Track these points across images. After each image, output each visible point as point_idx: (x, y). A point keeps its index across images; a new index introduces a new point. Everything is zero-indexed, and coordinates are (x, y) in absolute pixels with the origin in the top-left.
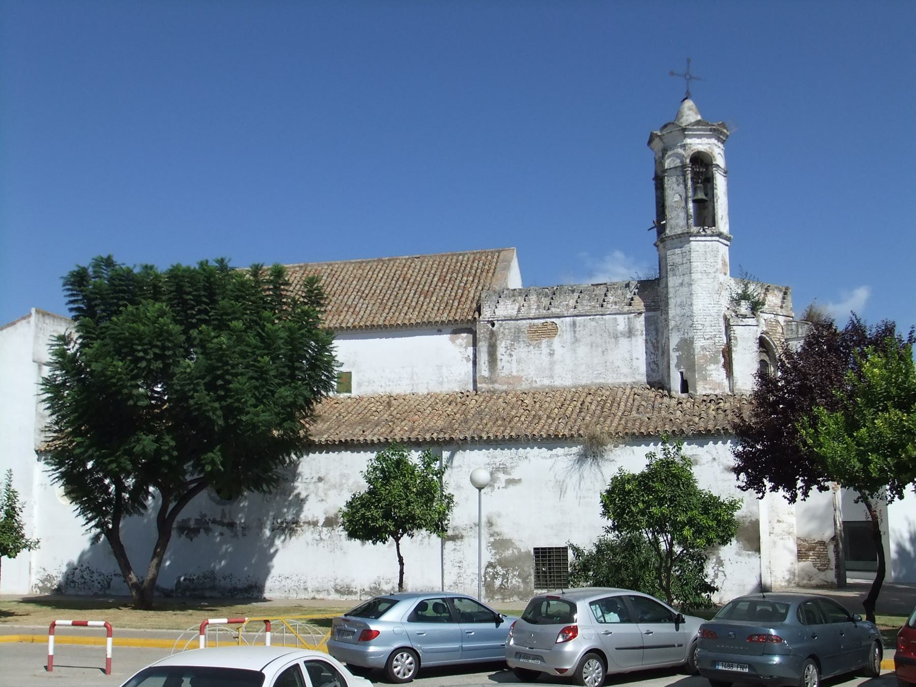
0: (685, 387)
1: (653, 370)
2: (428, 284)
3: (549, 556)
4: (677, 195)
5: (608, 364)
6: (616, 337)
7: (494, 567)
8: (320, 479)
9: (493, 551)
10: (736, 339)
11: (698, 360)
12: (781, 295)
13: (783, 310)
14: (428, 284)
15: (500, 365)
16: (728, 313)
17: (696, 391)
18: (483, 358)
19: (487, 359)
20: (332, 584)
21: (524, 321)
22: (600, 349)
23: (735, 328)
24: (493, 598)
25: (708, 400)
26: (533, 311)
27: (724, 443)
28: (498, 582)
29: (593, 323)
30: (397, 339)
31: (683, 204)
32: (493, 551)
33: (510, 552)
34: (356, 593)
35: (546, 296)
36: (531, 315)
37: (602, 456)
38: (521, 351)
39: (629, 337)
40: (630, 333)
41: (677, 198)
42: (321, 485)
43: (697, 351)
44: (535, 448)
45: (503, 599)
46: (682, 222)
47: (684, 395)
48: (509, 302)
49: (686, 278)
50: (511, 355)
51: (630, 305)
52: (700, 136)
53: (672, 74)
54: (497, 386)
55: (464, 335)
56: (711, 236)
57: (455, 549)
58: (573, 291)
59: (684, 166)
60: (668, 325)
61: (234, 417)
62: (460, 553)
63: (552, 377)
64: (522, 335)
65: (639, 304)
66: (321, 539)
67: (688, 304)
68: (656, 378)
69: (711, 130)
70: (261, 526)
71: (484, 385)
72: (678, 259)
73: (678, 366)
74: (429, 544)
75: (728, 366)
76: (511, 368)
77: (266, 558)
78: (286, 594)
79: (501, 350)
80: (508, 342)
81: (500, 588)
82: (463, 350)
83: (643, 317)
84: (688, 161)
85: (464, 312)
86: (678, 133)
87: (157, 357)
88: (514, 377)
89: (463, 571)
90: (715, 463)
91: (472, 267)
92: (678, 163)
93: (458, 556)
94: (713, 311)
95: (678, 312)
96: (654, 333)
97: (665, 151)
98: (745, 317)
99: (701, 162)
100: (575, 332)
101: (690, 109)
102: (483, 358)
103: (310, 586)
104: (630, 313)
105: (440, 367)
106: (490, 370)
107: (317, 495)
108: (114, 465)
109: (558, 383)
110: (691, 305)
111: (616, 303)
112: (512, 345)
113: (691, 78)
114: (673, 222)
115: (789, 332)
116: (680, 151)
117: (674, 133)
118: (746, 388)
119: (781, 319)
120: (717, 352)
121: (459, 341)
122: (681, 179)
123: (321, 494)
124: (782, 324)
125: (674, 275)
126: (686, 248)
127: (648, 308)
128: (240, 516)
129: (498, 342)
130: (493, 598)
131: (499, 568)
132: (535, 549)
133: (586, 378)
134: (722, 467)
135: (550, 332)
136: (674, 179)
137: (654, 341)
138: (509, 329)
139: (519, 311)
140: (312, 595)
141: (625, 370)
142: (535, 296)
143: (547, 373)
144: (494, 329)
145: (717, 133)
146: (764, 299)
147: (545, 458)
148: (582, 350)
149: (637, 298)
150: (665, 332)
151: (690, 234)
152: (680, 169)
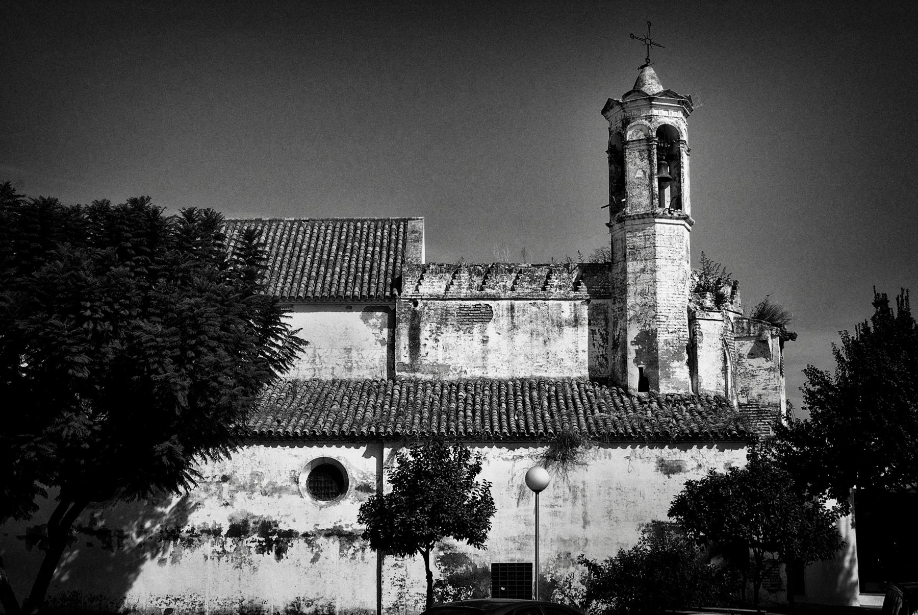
0: (644, 384)
2: (325, 253)
5: (550, 355)
6: (560, 326)
8: (225, 479)
9: (443, 568)
13: (733, 306)
14: (325, 253)
15: (423, 351)
17: (658, 390)
18: (403, 341)
19: (407, 343)
20: (237, 606)
21: (454, 302)
22: (541, 339)
25: (673, 400)
26: (464, 291)
29: (534, 309)
30: (303, 314)
31: (647, 182)
32: (443, 568)
35: (479, 274)
36: (462, 296)
38: (449, 335)
39: (575, 326)
41: (640, 174)
42: (225, 485)
43: (660, 345)
46: (645, 201)
47: (643, 394)
48: (436, 279)
50: (436, 340)
51: (576, 289)
52: (666, 108)
54: (419, 375)
55: (379, 314)
56: (677, 219)
57: (396, 565)
58: (510, 271)
59: (649, 139)
60: (624, 315)
61: (204, 399)
62: (403, 569)
63: (484, 367)
64: (450, 318)
66: (224, 551)
67: (650, 292)
68: (604, 373)
69: (679, 102)
71: (404, 374)
72: (639, 242)
73: (636, 361)
74: (363, 558)
76: (436, 356)
79: (424, 334)
80: (434, 325)
82: (378, 331)
84: (654, 134)
85: (379, 287)
87: (107, 317)
88: (439, 366)
89: (405, 590)
91: (375, 237)
92: (641, 135)
93: (399, 573)
95: (638, 301)
97: (626, 122)
99: (667, 134)
100: (513, 317)
101: (653, 78)
102: (403, 341)
104: (575, 298)
105: (348, 350)
106: (411, 357)
107: (220, 497)
109: (492, 375)
110: (655, 294)
111: (560, 287)
112: (438, 328)
114: (634, 200)
118: (711, 389)
120: (681, 347)
121: (372, 321)
123: (226, 496)
124: (733, 321)
125: (634, 259)
126: (649, 230)
127: (594, 295)
129: (422, 324)
132: (493, 565)
133: (524, 371)
135: (486, 316)
138: (435, 310)
139: (447, 289)
141: (569, 363)
142: (466, 274)
143: (479, 362)
144: (418, 308)
145: (685, 105)
147: (507, 459)
148: (521, 338)
150: (620, 322)
151: (655, 215)
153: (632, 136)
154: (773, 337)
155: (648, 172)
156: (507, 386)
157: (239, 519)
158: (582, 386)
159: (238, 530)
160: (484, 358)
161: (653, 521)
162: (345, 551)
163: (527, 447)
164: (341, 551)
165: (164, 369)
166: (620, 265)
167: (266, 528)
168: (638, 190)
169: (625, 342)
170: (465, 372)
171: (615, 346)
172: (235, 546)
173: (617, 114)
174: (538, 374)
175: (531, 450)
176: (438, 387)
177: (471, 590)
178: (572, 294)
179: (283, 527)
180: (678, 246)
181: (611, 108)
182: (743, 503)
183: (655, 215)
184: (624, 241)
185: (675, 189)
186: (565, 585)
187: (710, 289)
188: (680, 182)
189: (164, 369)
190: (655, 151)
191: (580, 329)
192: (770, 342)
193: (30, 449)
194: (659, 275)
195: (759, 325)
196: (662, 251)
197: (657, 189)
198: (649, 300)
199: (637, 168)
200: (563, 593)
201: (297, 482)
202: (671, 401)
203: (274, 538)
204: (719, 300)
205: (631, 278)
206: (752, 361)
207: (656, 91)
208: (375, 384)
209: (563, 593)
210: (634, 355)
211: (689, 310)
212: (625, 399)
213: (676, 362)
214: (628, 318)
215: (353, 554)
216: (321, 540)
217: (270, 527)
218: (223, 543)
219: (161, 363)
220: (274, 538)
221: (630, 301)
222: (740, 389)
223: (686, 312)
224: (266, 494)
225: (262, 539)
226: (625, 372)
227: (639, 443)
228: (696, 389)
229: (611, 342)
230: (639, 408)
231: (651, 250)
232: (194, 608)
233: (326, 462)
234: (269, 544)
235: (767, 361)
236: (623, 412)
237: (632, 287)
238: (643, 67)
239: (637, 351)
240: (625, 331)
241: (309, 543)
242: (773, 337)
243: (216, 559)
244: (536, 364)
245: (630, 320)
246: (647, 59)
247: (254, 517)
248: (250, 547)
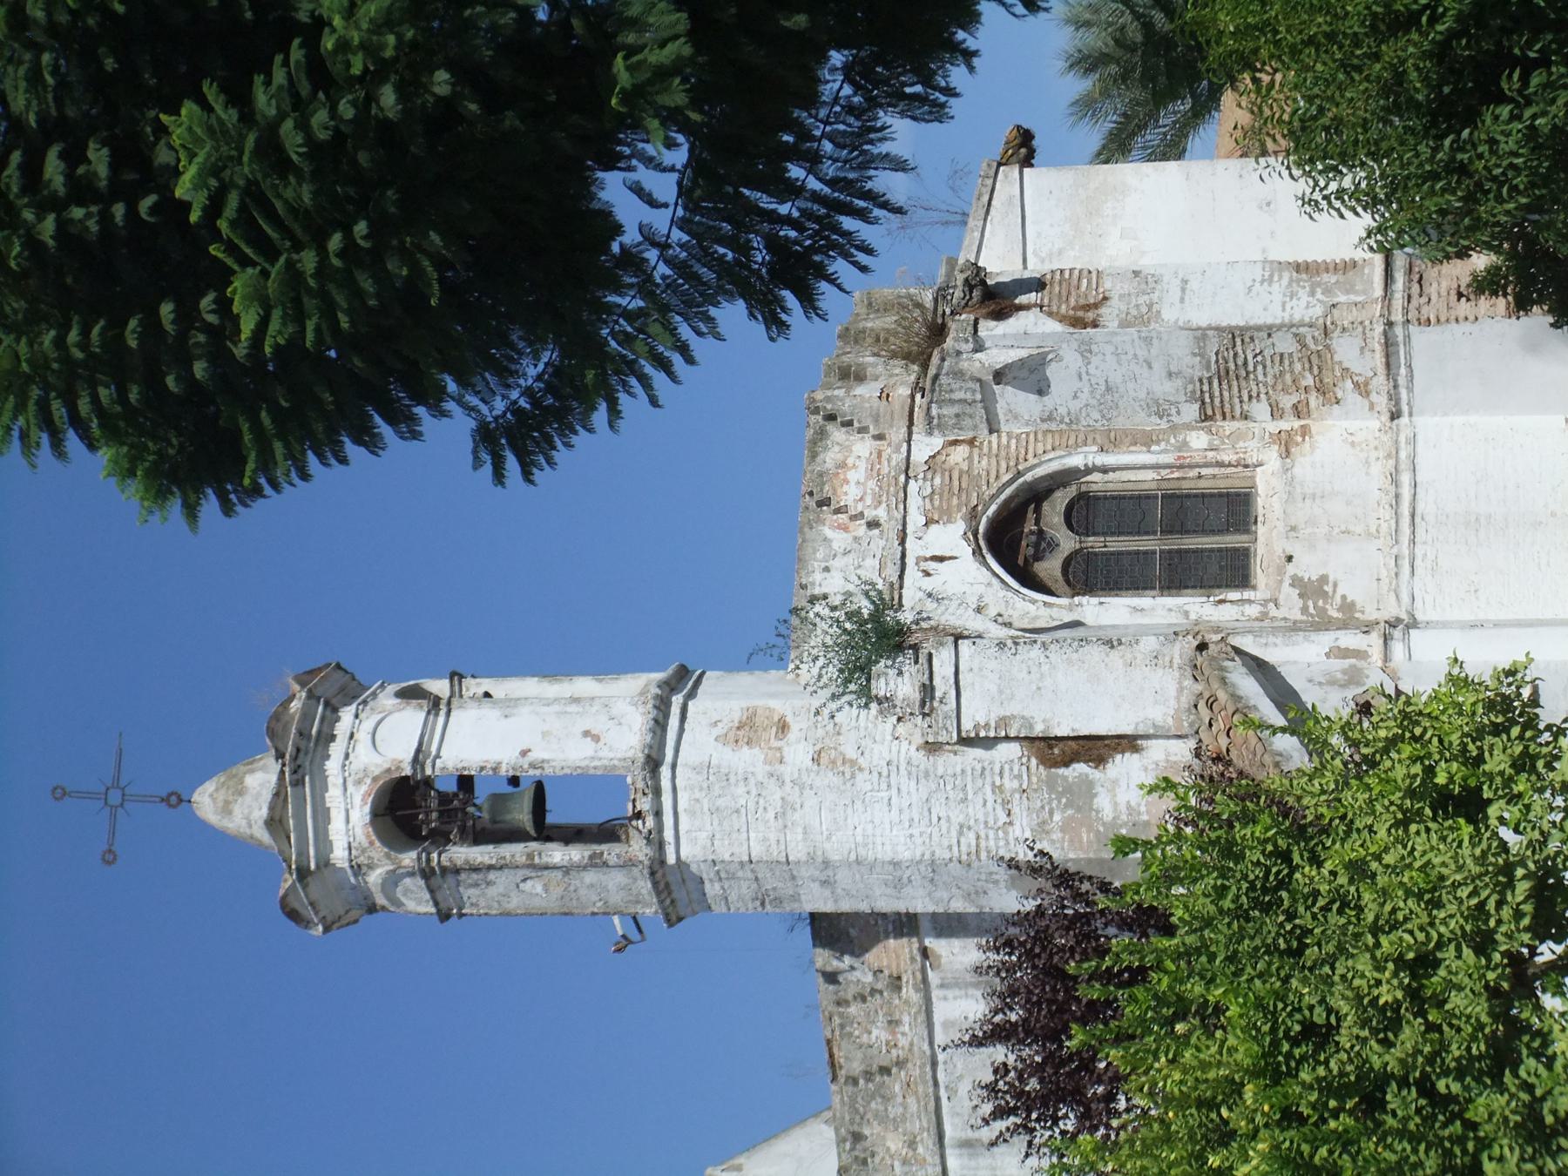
10: (1004, 721)
12: (837, 434)
23: (967, 725)
49: (804, 872)
52: (322, 816)
53: (109, 857)
56: (657, 792)
69: (298, 783)
92: (416, 884)
94: (914, 793)
98: (928, 690)
110: (896, 864)
111: (893, 1023)
113: (116, 783)
115: (967, 422)
118: (1172, 689)
119: (925, 446)
120: (1051, 784)
124: (937, 442)
125: (795, 898)
136: (472, 892)
153: (419, 901)
155: (528, 872)
178: (909, 992)
180: (741, 790)
194: (836, 850)
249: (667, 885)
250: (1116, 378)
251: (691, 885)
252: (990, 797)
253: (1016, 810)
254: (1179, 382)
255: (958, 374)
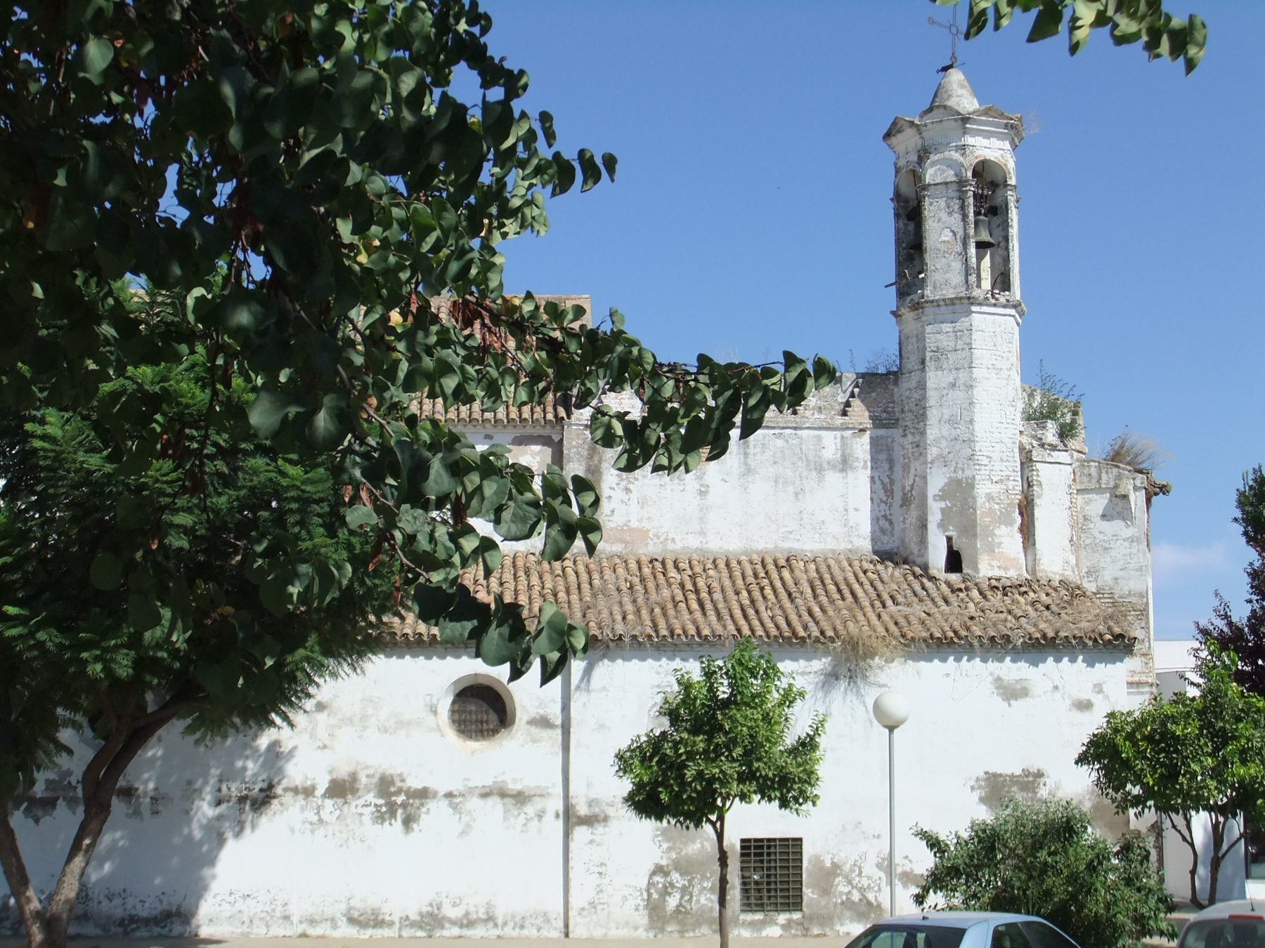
0: (954, 562)
1: (883, 531)
3: (769, 854)
4: (947, 232)
6: (820, 470)
7: (666, 874)
9: (665, 845)
10: (1040, 484)
11: (982, 519)
16: (1025, 440)
17: (976, 570)
22: (791, 489)
23: (1039, 466)
24: (662, 930)
27: (1073, 660)
28: (672, 902)
29: (780, 443)
31: (959, 248)
32: (665, 845)
33: (697, 846)
34: (391, 924)
37: (865, 677)
39: (843, 470)
40: (845, 464)
41: (947, 236)
43: (980, 501)
44: (408, 657)
45: (682, 932)
46: (956, 277)
47: (954, 577)
49: (963, 376)
50: (627, 490)
51: (844, 414)
52: (987, 135)
55: (536, 448)
56: (1004, 306)
57: (591, 842)
59: (961, 183)
63: (702, 533)
65: (860, 413)
66: (321, 821)
67: (964, 418)
68: (889, 544)
69: (1006, 126)
70: (190, 792)
72: (946, 342)
73: (942, 525)
74: (540, 831)
75: (1027, 531)
77: (201, 857)
78: (245, 929)
81: (677, 911)
83: (866, 438)
84: (970, 174)
86: (953, 124)
88: (631, 530)
89: (607, 881)
90: (1058, 695)
92: (950, 176)
95: (945, 433)
96: (886, 466)
97: (923, 155)
100: (746, 454)
101: (962, 87)
103: (296, 912)
107: (313, 736)
108: (99, 667)
110: (971, 421)
111: (820, 410)
115: (1085, 479)
116: (956, 156)
117: (945, 124)
122: (956, 205)
125: (940, 368)
126: (963, 323)
127: (878, 422)
128: (146, 776)
130: (662, 930)
131: (675, 876)
132: (743, 841)
134: (1068, 702)
136: (942, 203)
137: (886, 480)
140: (300, 931)
145: (1013, 131)
146: (1074, 421)
149: (856, 403)
150: (915, 465)
151: (971, 300)
152: (955, 187)
154: (1136, 489)
155: (960, 233)
156: (739, 563)
157: (343, 772)
158: (856, 563)
159: (341, 789)
160: (701, 519)
161: (986, 773)
162: (512, 819)
163: (795, 659)
164: (505, 819)
165: (309, 532)
166: (915, 377)
167: (385, 786)
168: (944, 260)
169: (924, 497)
170: (673, 540)
171: (906, 502)
172: (338, 812)
173: (907, 141)
174: (787, 545)
175: (802, 663)
176: (633, 566)
177: (708, 879)
179: (414, 783)
181: (899, 131)
182: (1206, 744)
183: (971, 300)
184: (921, 338)
185: (998, 259)
186: (852, 871)
187: (1052, 414)
188: (1007, 248)
189: (309, 532)
190: (971, 200)
191: (851, 475)
192: (1132, 497)
193: (97, 659)
194: (978, 392)
195: (1115, 470)
196: (982, 355)
197: (974, 260)
198: (961, 431)
199: (943, 226)
200: (849, 882)
201: (435, 713)
202: (997, 588)
203: (400, 799)
204: (1066, 432)
205: (932, 397)
206: (1106, 526)
207: (971, 110)
208: (532, 558)
209: (849, 882)
210: (938, 516)
211: (1022, 449)
212: (928, 584)
213: (1003, 527)
214: (929, 458)
215: (525, 825)
216: (474, 803)
217: (392, 783)
218: (319, 808)
219: (302, 524)
220: (400, 799)
221: (932, 432)
222: (1085, 570)
223: (1017, 450)
224: (386, 731)
225: (381, 802)
226: (923, 541)
227: (965, 653)
228: (1033, 572)
229: (898, 496)
230: (952, 598)
231: (966, 352)
232: (274, 910)
233: (480, 681)
234: (392, 809)
235: (1128, 526)
236: (929, 603)
237: (934, 411)
238: (945, 69)
239: (943, 511)
240: (924, 478)
241: (455, 807)
242: (1136, 489)
243: (308, 832)
244: (783, 530)
245: (932, 463)
246: (953, 57)
247: (367, 767)
248: (361, 815)
249: (954, 304)
250: (1113, 553)
251: (950, 317)
252: (1004, 474)
253: (998, 486)
254: (1111, 583)
255: (1119, 477)
